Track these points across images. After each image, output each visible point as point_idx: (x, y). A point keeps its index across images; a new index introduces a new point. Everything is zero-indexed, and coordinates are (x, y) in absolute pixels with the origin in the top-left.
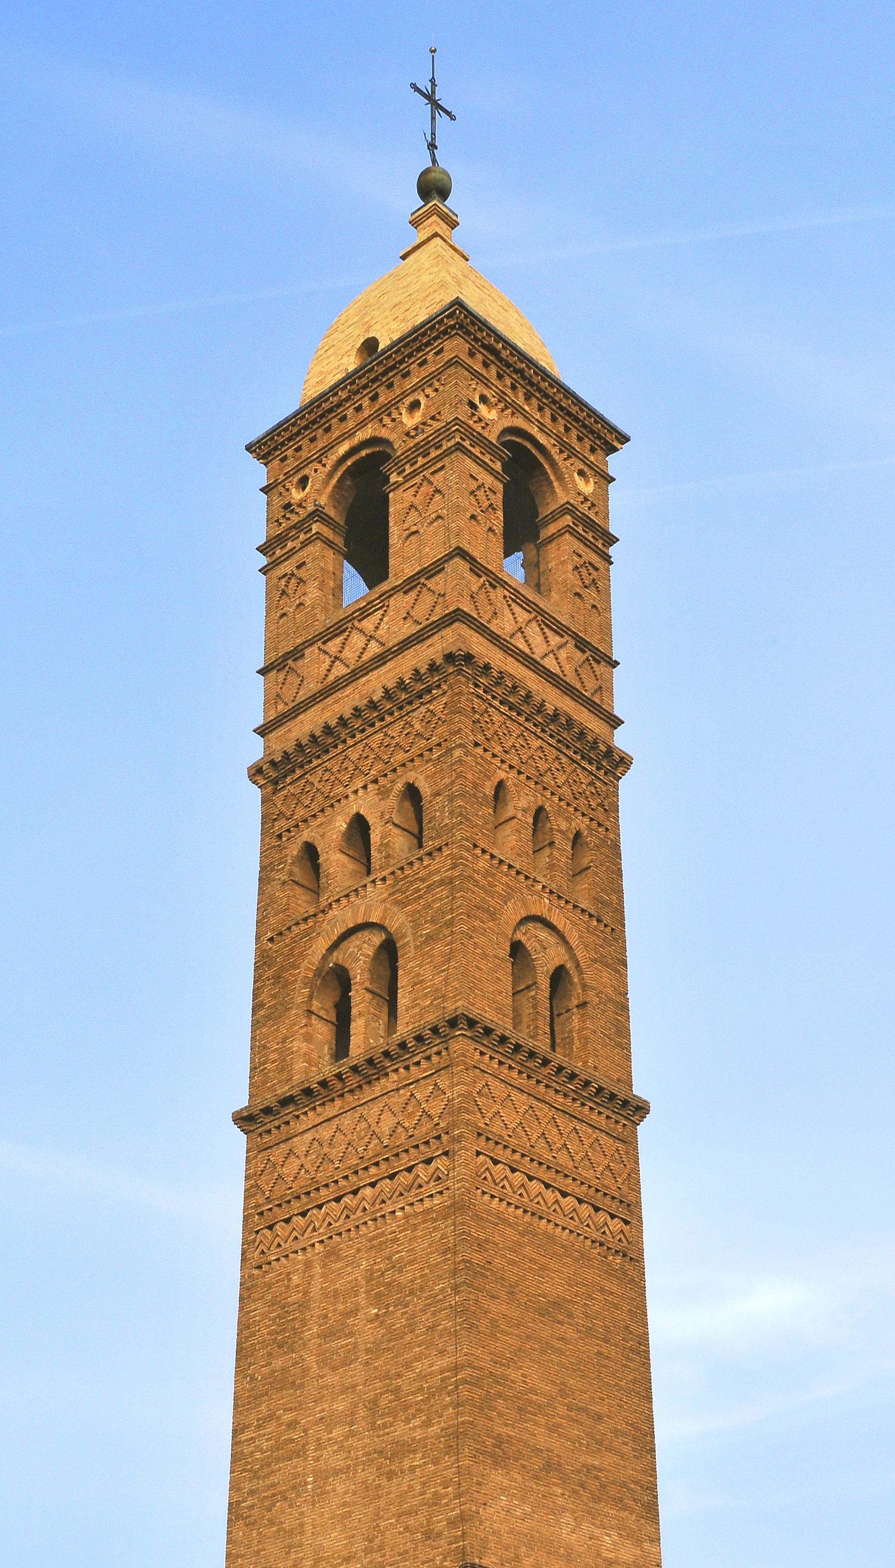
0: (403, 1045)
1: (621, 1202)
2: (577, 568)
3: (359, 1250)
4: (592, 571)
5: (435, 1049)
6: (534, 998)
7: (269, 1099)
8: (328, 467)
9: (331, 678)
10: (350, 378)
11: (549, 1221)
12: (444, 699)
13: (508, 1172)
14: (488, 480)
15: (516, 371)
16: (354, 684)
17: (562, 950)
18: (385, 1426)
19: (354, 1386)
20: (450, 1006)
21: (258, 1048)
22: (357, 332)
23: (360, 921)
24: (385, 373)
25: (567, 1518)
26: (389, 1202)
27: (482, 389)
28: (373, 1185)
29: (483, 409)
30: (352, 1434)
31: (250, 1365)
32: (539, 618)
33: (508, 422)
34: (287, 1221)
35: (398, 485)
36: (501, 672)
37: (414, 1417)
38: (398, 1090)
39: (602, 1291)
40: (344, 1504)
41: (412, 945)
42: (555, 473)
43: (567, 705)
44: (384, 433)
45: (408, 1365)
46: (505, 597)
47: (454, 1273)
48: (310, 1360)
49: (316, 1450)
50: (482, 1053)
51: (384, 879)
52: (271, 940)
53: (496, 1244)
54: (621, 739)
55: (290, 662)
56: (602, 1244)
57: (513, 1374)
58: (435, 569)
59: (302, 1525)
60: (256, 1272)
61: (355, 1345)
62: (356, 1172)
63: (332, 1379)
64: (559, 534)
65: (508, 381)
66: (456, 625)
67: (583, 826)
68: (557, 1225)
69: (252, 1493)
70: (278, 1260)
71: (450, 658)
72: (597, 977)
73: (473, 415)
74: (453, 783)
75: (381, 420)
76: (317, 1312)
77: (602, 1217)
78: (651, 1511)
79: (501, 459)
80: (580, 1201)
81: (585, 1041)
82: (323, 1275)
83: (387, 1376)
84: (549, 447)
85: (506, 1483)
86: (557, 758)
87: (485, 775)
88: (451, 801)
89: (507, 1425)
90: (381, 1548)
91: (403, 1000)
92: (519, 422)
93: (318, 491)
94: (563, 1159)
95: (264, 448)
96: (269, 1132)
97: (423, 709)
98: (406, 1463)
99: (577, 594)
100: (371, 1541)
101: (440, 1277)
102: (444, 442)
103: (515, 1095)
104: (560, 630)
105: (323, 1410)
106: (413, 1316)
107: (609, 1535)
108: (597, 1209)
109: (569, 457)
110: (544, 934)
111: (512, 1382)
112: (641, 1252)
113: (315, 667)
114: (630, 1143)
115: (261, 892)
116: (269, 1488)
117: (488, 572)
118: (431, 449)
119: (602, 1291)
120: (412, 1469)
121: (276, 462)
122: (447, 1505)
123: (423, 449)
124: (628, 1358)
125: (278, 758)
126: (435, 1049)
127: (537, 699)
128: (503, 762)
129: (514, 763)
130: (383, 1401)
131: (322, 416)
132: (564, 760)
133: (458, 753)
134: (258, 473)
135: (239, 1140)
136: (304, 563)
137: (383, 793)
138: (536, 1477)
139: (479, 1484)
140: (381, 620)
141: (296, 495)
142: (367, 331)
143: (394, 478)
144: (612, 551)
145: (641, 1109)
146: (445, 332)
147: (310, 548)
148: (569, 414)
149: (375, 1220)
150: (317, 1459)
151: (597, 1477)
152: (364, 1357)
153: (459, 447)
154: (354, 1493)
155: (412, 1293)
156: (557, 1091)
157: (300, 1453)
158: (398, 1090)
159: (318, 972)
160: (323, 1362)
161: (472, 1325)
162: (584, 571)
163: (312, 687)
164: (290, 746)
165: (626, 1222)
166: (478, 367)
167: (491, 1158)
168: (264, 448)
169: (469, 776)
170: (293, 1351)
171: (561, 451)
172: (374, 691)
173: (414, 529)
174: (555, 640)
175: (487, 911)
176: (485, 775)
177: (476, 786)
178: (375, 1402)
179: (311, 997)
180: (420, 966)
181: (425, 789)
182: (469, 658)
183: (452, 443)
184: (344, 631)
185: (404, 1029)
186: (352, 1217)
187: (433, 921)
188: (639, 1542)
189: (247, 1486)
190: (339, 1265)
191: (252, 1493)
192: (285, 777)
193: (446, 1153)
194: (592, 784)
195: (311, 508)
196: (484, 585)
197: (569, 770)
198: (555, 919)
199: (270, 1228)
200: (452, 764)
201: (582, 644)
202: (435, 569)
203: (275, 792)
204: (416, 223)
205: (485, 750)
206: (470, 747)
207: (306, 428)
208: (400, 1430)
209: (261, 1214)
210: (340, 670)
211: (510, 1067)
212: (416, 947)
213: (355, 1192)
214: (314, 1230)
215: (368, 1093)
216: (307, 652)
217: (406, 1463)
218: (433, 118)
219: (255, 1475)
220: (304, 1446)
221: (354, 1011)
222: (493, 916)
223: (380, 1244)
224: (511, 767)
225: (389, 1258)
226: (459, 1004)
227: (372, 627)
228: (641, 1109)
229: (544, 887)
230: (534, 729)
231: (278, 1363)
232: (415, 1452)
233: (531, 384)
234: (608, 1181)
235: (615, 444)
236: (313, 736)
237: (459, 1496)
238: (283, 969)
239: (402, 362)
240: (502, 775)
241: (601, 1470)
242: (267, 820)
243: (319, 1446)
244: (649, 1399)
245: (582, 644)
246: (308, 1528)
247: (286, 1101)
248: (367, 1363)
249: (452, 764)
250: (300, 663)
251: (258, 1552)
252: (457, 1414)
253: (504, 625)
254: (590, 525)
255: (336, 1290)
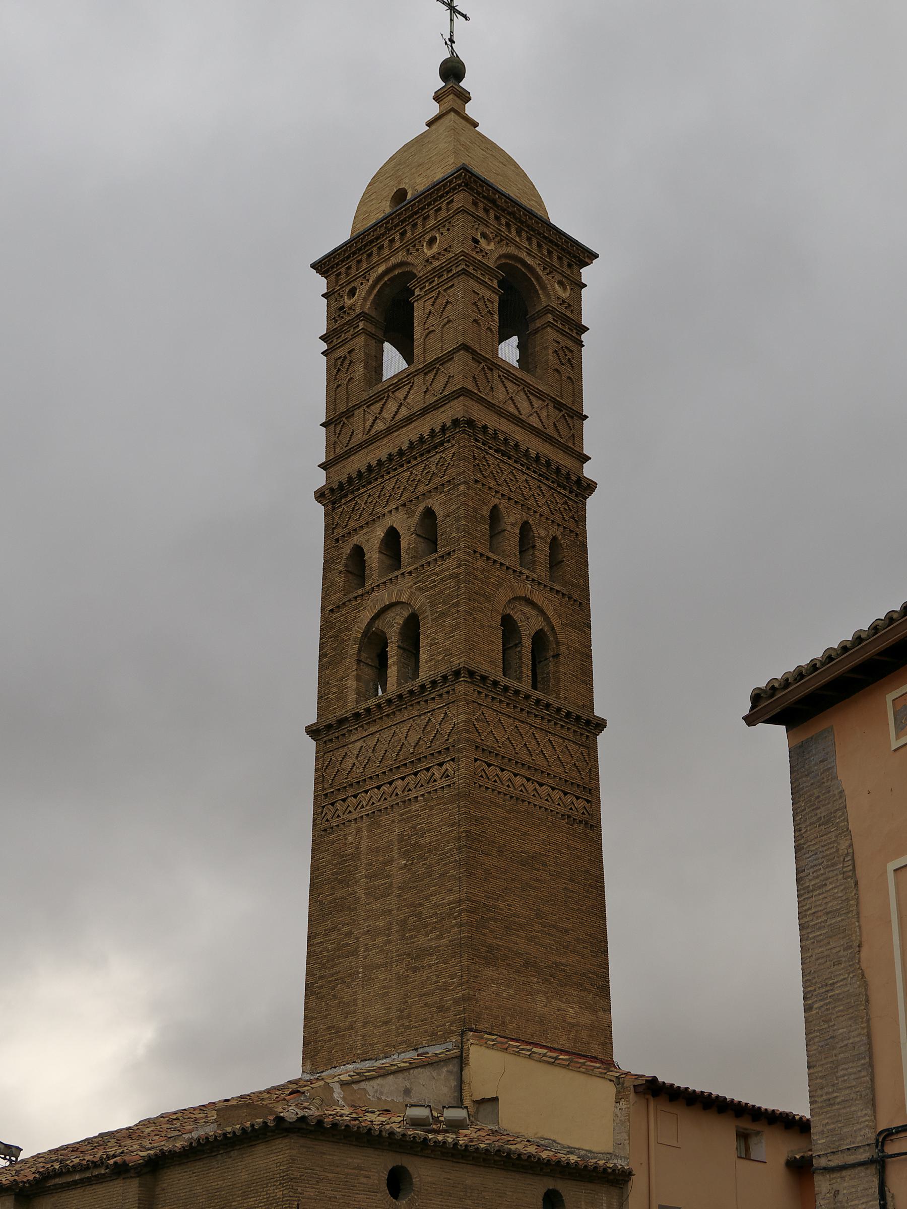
0: (423, 687)
1: (584, 788)
2: (556, 351)
3: (393, 821)
4: (567, 352)
5: (446, 690)
6: (519, 652)
7: (332, 719)
8: (371, 282)
9: (373, 432)
10: (387, 219)
11: (529, 803)
12: (453, 450)
13: (499, 772)
14: (487, 294)
15: (510, 214)
16: (389, 437)
17: (541, 619)
18: (411, 937)
19: (390, 911)
20: (456, 661)
21: (323, 683)
22: (392, 183)
23: (394, 600)
24: (411, 216)
25: (541, 997)
26: (414, 791)
27: (482, 228)
28: (403, 779)
29: (483, 242)
30: (389, 942)
31: (320, 894)
32: (526, 389)
33: (504, 250)
34: (344, 800)
35: (420, 297)
36: (495, 430)
37: (431, 932)
38: (420, 715)
39: (569, 847)
40: (384, 987)
41: (430, 618)
42: (540, 284)
43: (546, 450)
44: (410, 259)
45: (427, 898)
46: (499, 376)
47: (459, 839)
48: (361, 893)
49: (364, 951)
50: (479, 693)
51: (410, 573)
52: (332, 611)
53: (489, 819)
54: (589, 471)
55: (344, 419)
56: (569, 816)
57: (502, 905)
58: (444, 360)
59: (355, 1000)
60: (323, 833)
61: (391, 884)
62: (391, 770)
63: (376, 906)
64: (543, 328)
65: (503, 221)
66: (462, 398)
67: (558, 533)
68: (535, 805)
69: (321, 978)
70: (338, 826)
71: (456, 422)
72: (566, 636)
73: (476, 247)
74: (459, 508)
75: (408, 250)
76: (365, 861)
77: (569, 799)
78: (604, 991)
79: (497, 277)
80: (553, 789)
81: (558, 680)
82: (369, 837)
83: (412, 905)
84: (535, 266)
85: (496, 975)
86: (539, 487)
87: (483, 502)
88: (457, 521)
89: (497, 938)
90: (409, 1016)
91: (423, 656)
92: (512, 250)
93: (361, 300)
94: (540, 761)
95: (322, 266)
96: (331, 740)
97: (438, 456)
98: (426, 963)
99: (557, 371)
100: (402, 1012)
101: (449, 842)
102: (453, 268)
103: (503, 719)
104: (541, 396)
105: (369, 926)
106: (430, 867)
107: (571, 1007)
108: (565, 794)
109: (551, 272)
110: (527, 609)
111: (501, 909)
112: (599, 820)
113: (359, 426)
114: (592, 749)
115: (325, 578)
116: (332, 975)
117: (486, 360)
118: (443, 274)
119: (569, 847)
120: (430, 966)
121: (333, 277)
122: (452, 990)
123: (438, 272)
124: (587, 891)
125: (335, 486)
126: (446, 690)
127: (523, 448)
128: (497, 492)
129: (505, 493)
130: (411, 921)
131: (365, 246)
132: (544, 487)
133: (462, 487)
134: (321, 284)
135: (311, 745)
136: (353, 349)
137: (410, 514)
138: (519, 972)
139: (476, 977)
140: (409, 392)
141: (348, 302)
142: (399, 183)
143: (417, 292)
144: (584, 337)
145: (601, 725)
146: (454, 189)
147: (357, 340)
148: (551, 241)
149: (404, 802)
150: (365, 958)
151: (564, 970)
152: (396, 892)
153: (465, 272)
154: (391, 980)
155: (430, 851)
156: (536, 716)
157: (354, 953)
158: (420, 715)
159: (365, 634)
160: (368, 895)
161: (471, 874)
162: (561, 353)
163: (359, 437)
164: (344, 478)
165: (588, 801)
166: (481, 213)
167: (486, 762)
168: (322, 266)
169: (471, 504)
170: (349, 887)
171: (545, 269)
172: (403, 443)
173: (432, 329)
174: (537, 403)
175: (484, 596)
176: (483, 502)
177: (475, 510)
178: (404, 921)
179: (360, 650)
180: (436, 633)
181: (439, 512)
182: (471, 423)
183: (460, 268)
184: (382, 399)
185: (424, 675)
186: (389, 799)
187: (444, 603)
188: (595, 1012)
189: (318, 974)
190: (379, 831)
191: (321, 978)
192: (341, 499)
193: (453, 760)
194: (566, 503)
195: (358, 311)
196: (483, 368)
197: (547, 495)
198: (537, 599)
199: (333, 804)
200: (459, 496)
201: (559, 406)
202: (444, 360)
203: (334, 509)
204: (438, 98)
205: (483, 485)
206: (472, 483)
207: (354, 253)
208: (422, 940)
209: (326, 795)
210: (380, 426)
211: (501, 701)
212: (433, 620)
213: (390, 783)
214: (362, 807)
215: (398, 718)
216: (356, 412)
217: (426, 963)
218: (452, 20)
219: (323, 966)
220: (356, 949)
221: (390, 661)
222: (488, 598)
223: (409, 818)
224: (503, 495)
225: (414, 827)
226: (462, 660)
227: (402, 397)
228: (601, 725)
229: (527, 577)
230: (520, 467)
231: (338, 894)
232: (432, 955)
233: (522, 222)
234: (575, 774)
235: (587, 260)
236: (359, 472)
237: (461, 985)
238: (340, 631)
239: (423, 208)
240: (496, 501)
241: (566, 966)
242: (330, 528)
243: (367, 949)
244: (604, 918)
245: (559, 406)
246: (360, 1002)
247: (341, 721)
248: (399, 896)
249: (459, 496)
250: (351, 420)
251: (326, 1016)
252: (460, 932)
253: (500, 395)
254: (566, 320)
255: (377, 847)
